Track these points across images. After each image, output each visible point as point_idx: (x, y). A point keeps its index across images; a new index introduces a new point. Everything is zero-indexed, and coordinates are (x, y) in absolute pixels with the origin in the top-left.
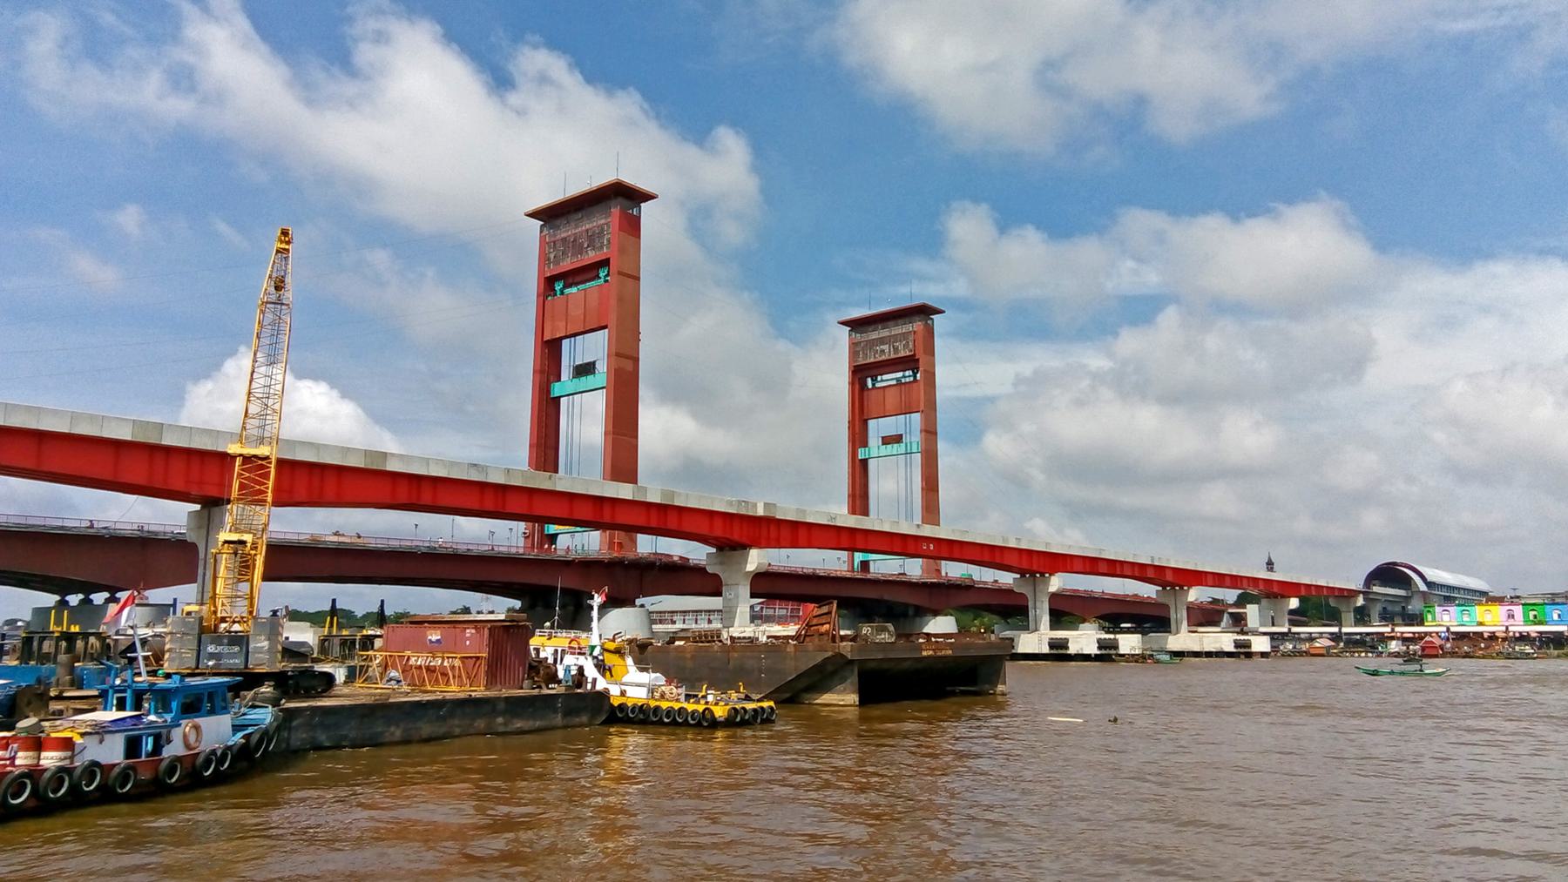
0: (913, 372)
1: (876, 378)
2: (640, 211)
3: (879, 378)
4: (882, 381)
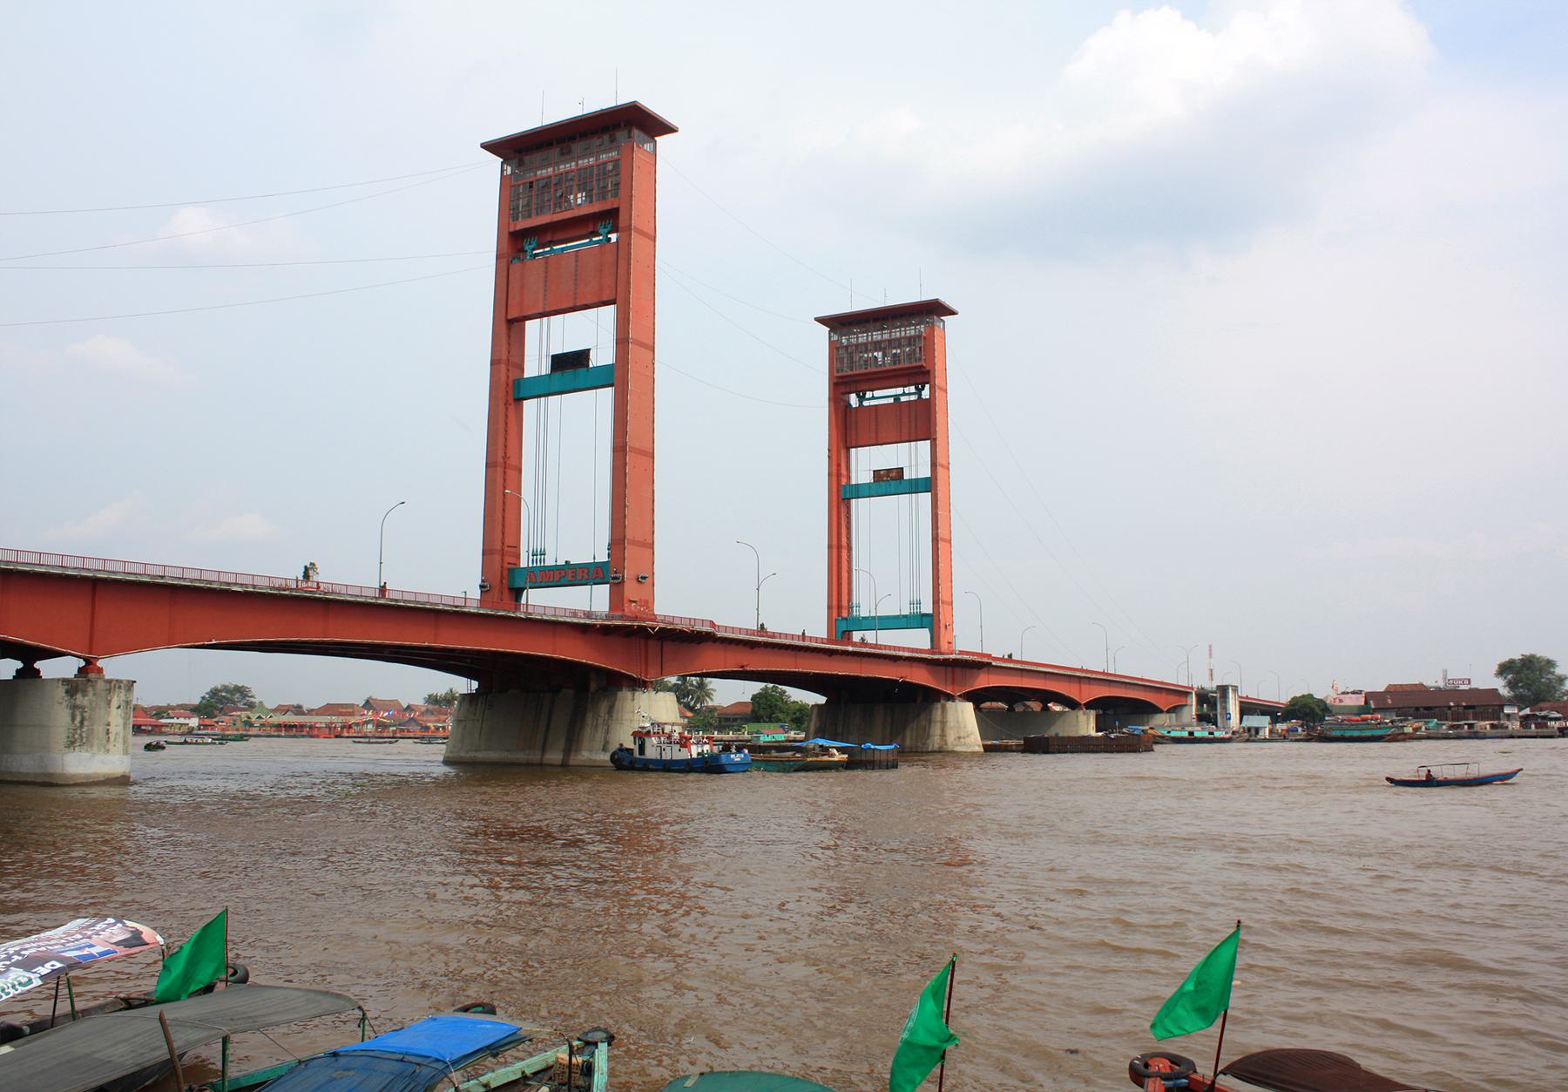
0: (917, 388)
1: (864, 395)
2: (502, 171)
3: (869, 395)
4: (873, 398)
